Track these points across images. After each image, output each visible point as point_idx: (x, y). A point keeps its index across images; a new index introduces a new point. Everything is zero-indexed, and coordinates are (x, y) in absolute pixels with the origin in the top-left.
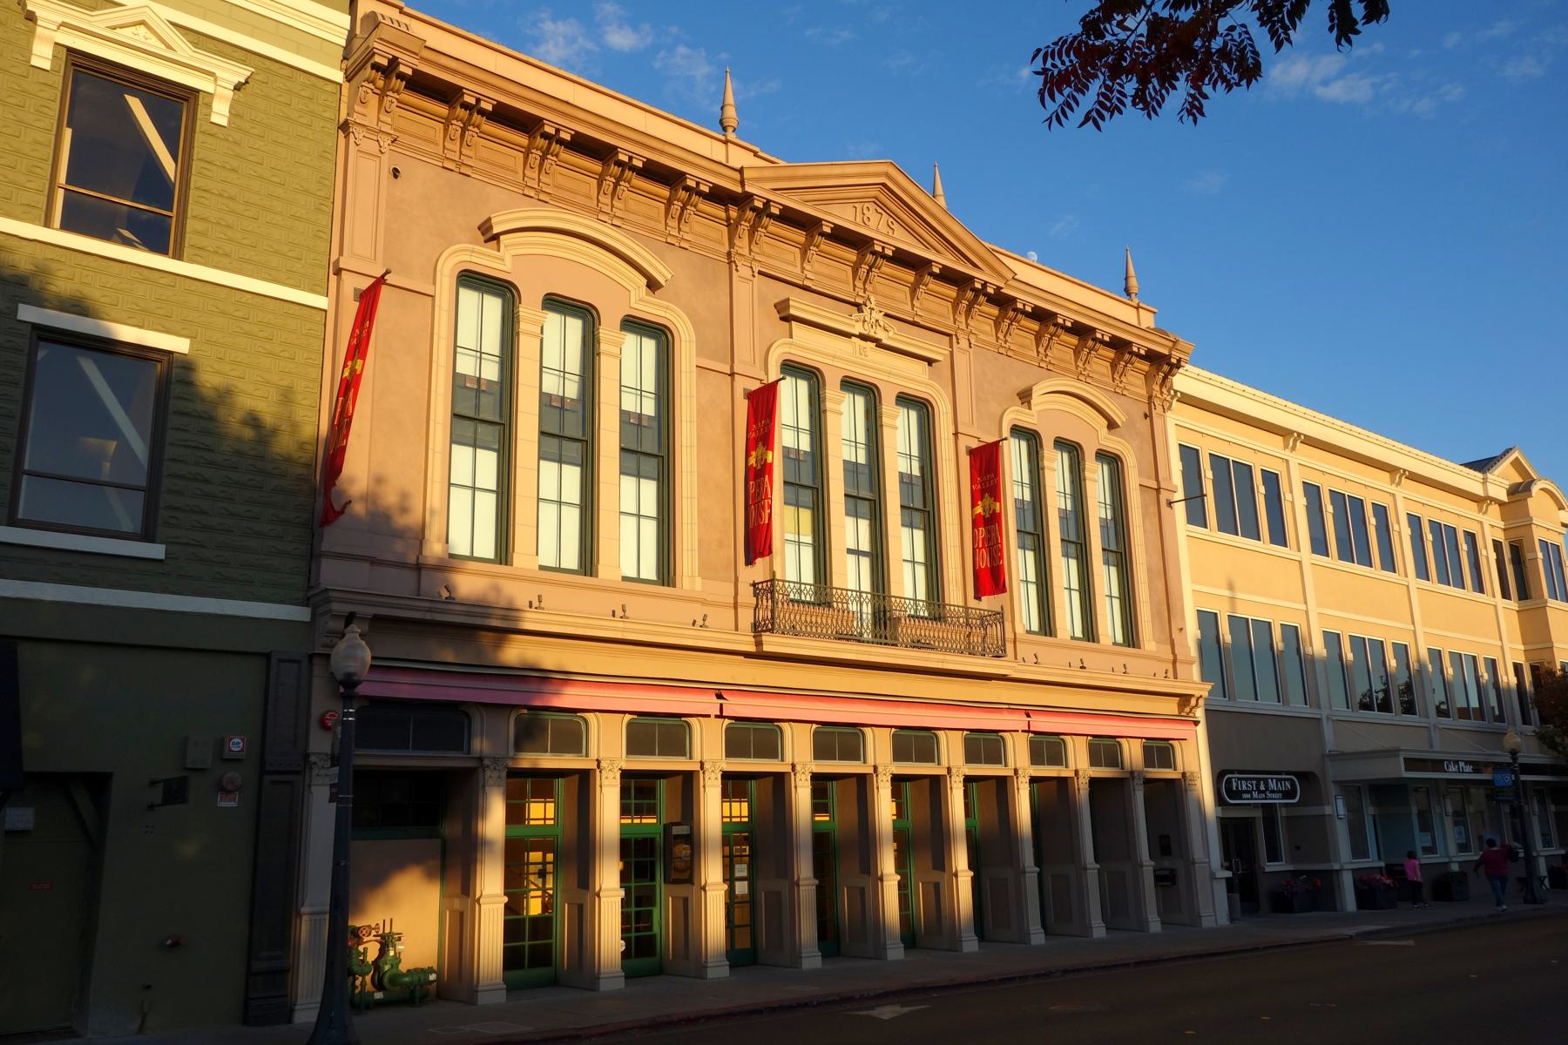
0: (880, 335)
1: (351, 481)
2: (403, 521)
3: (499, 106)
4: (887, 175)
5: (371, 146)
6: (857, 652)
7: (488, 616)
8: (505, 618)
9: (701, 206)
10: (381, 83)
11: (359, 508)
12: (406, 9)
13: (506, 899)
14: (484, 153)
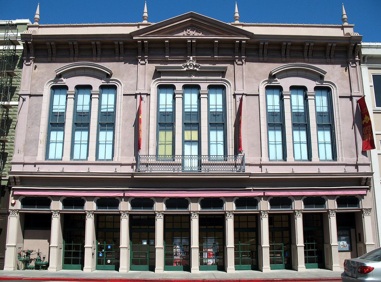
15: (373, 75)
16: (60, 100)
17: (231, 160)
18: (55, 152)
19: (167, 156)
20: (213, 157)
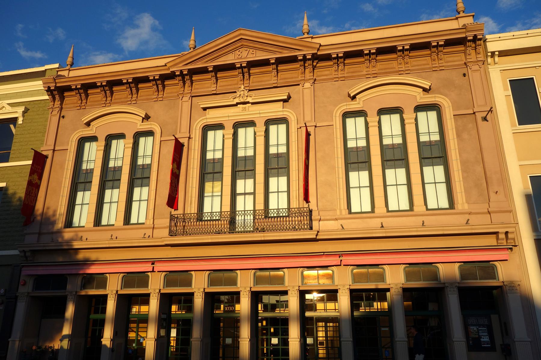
0: (250, 100)
1: (38, 210)
2: (52, 219)
3: (378, 49)
4: (241, 34)
5: (477, 67)
6: (211, 239)
7: (62, 246)
8: (68, 245)
9: (444, 51)
10: (474, 45)
11: (39, 218)
12: (314, 36)
13: (102, 340)
14: (415, 63)
15: (510, 81)
16: (356, 128)
17: (243, 216)
18: (361, 201)
19: (193, 215)
20: (226, 213)
